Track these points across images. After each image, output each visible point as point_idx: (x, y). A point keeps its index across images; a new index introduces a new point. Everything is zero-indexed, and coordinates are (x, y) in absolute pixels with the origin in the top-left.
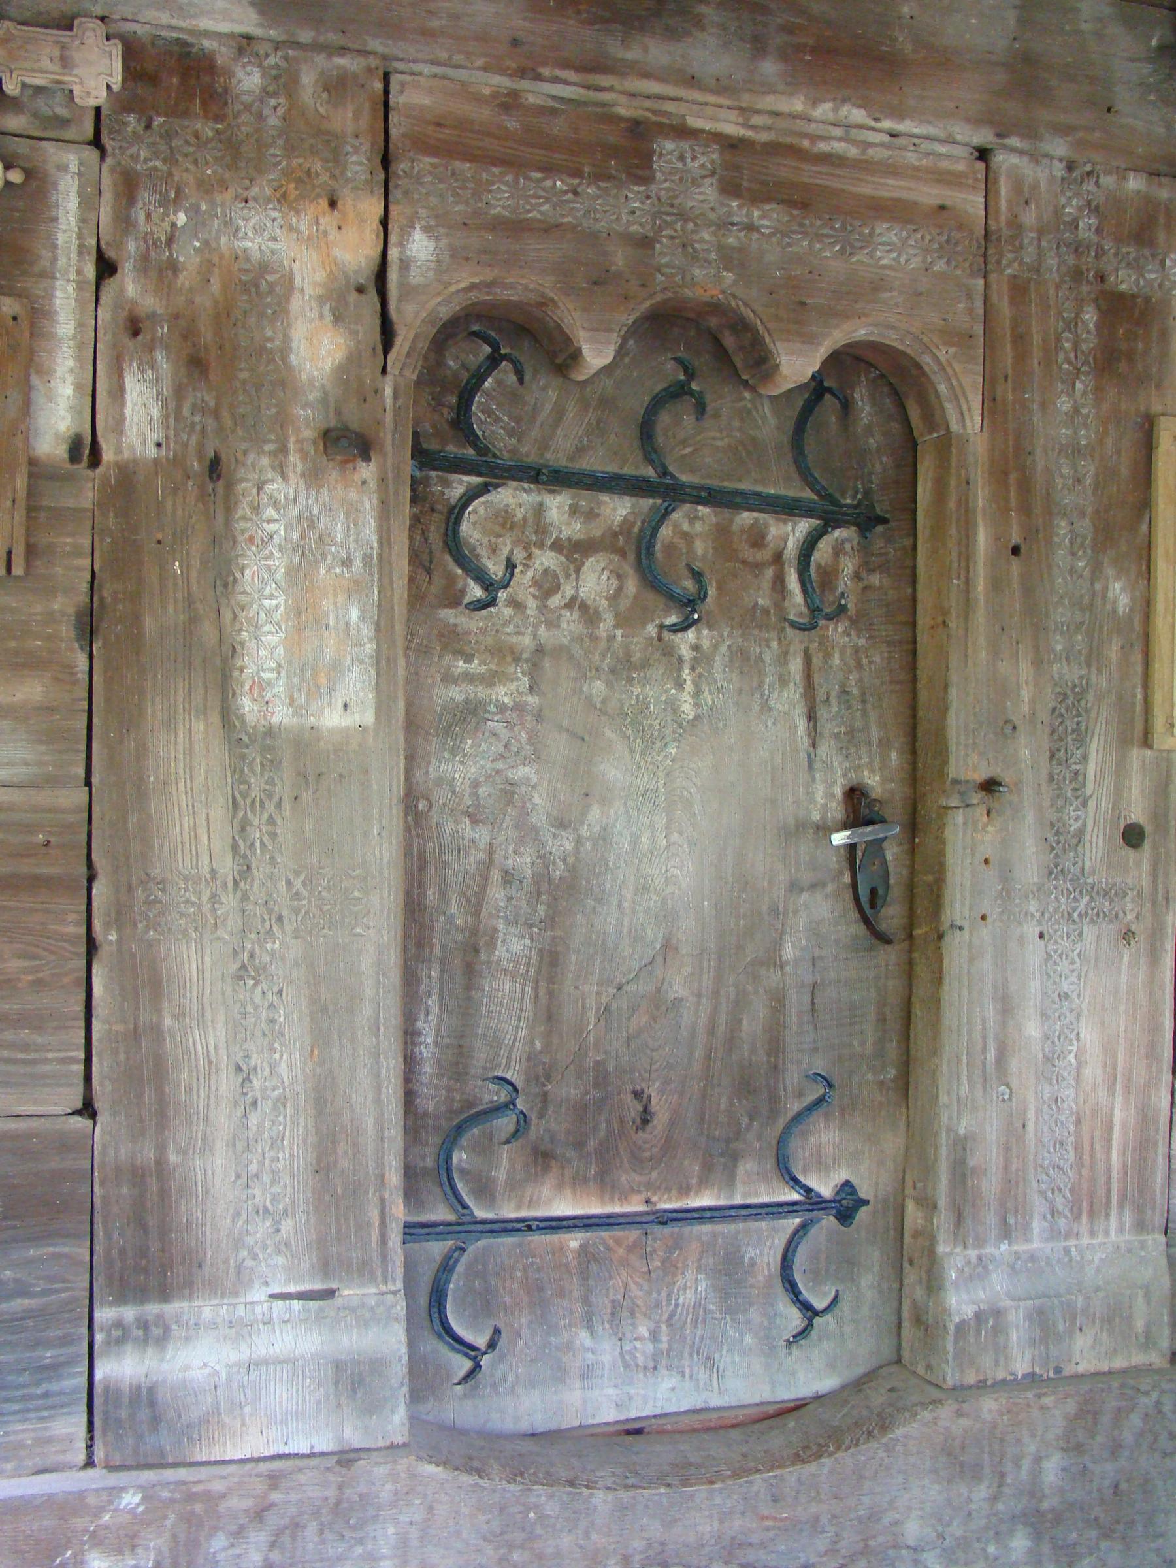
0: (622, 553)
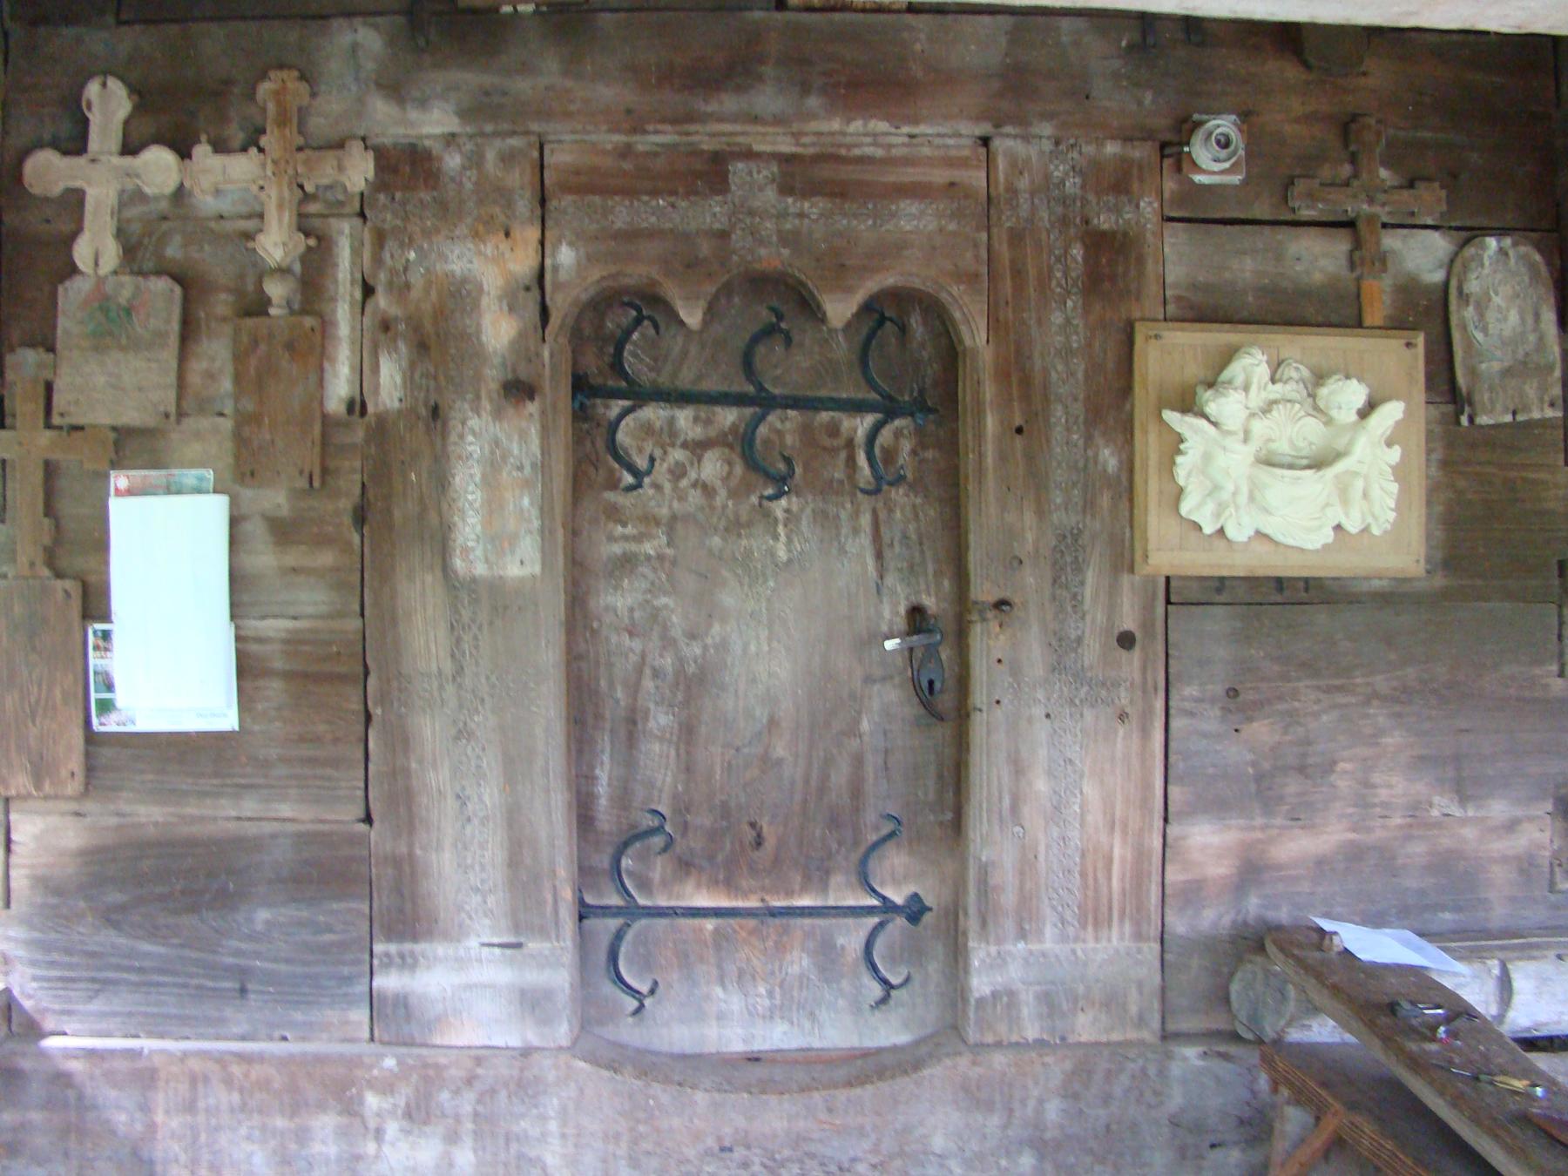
0: (731, 447)
